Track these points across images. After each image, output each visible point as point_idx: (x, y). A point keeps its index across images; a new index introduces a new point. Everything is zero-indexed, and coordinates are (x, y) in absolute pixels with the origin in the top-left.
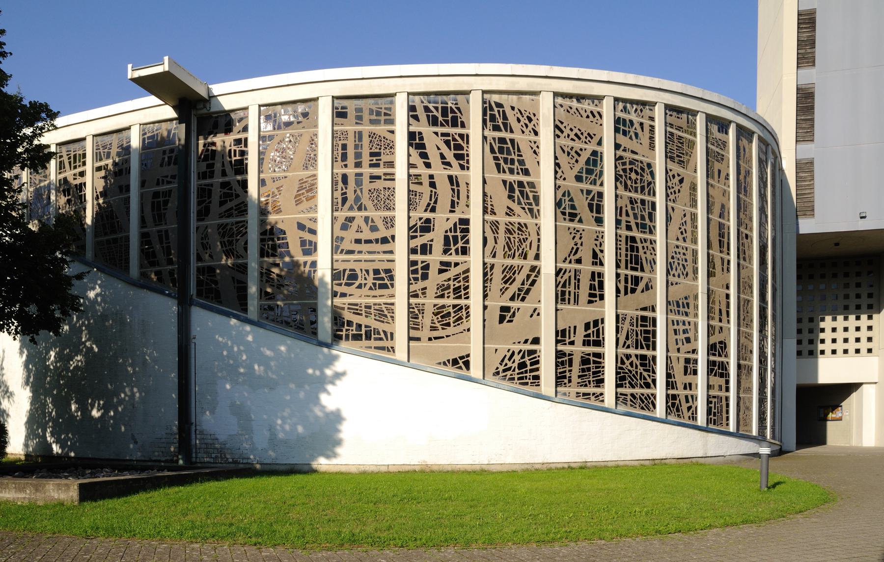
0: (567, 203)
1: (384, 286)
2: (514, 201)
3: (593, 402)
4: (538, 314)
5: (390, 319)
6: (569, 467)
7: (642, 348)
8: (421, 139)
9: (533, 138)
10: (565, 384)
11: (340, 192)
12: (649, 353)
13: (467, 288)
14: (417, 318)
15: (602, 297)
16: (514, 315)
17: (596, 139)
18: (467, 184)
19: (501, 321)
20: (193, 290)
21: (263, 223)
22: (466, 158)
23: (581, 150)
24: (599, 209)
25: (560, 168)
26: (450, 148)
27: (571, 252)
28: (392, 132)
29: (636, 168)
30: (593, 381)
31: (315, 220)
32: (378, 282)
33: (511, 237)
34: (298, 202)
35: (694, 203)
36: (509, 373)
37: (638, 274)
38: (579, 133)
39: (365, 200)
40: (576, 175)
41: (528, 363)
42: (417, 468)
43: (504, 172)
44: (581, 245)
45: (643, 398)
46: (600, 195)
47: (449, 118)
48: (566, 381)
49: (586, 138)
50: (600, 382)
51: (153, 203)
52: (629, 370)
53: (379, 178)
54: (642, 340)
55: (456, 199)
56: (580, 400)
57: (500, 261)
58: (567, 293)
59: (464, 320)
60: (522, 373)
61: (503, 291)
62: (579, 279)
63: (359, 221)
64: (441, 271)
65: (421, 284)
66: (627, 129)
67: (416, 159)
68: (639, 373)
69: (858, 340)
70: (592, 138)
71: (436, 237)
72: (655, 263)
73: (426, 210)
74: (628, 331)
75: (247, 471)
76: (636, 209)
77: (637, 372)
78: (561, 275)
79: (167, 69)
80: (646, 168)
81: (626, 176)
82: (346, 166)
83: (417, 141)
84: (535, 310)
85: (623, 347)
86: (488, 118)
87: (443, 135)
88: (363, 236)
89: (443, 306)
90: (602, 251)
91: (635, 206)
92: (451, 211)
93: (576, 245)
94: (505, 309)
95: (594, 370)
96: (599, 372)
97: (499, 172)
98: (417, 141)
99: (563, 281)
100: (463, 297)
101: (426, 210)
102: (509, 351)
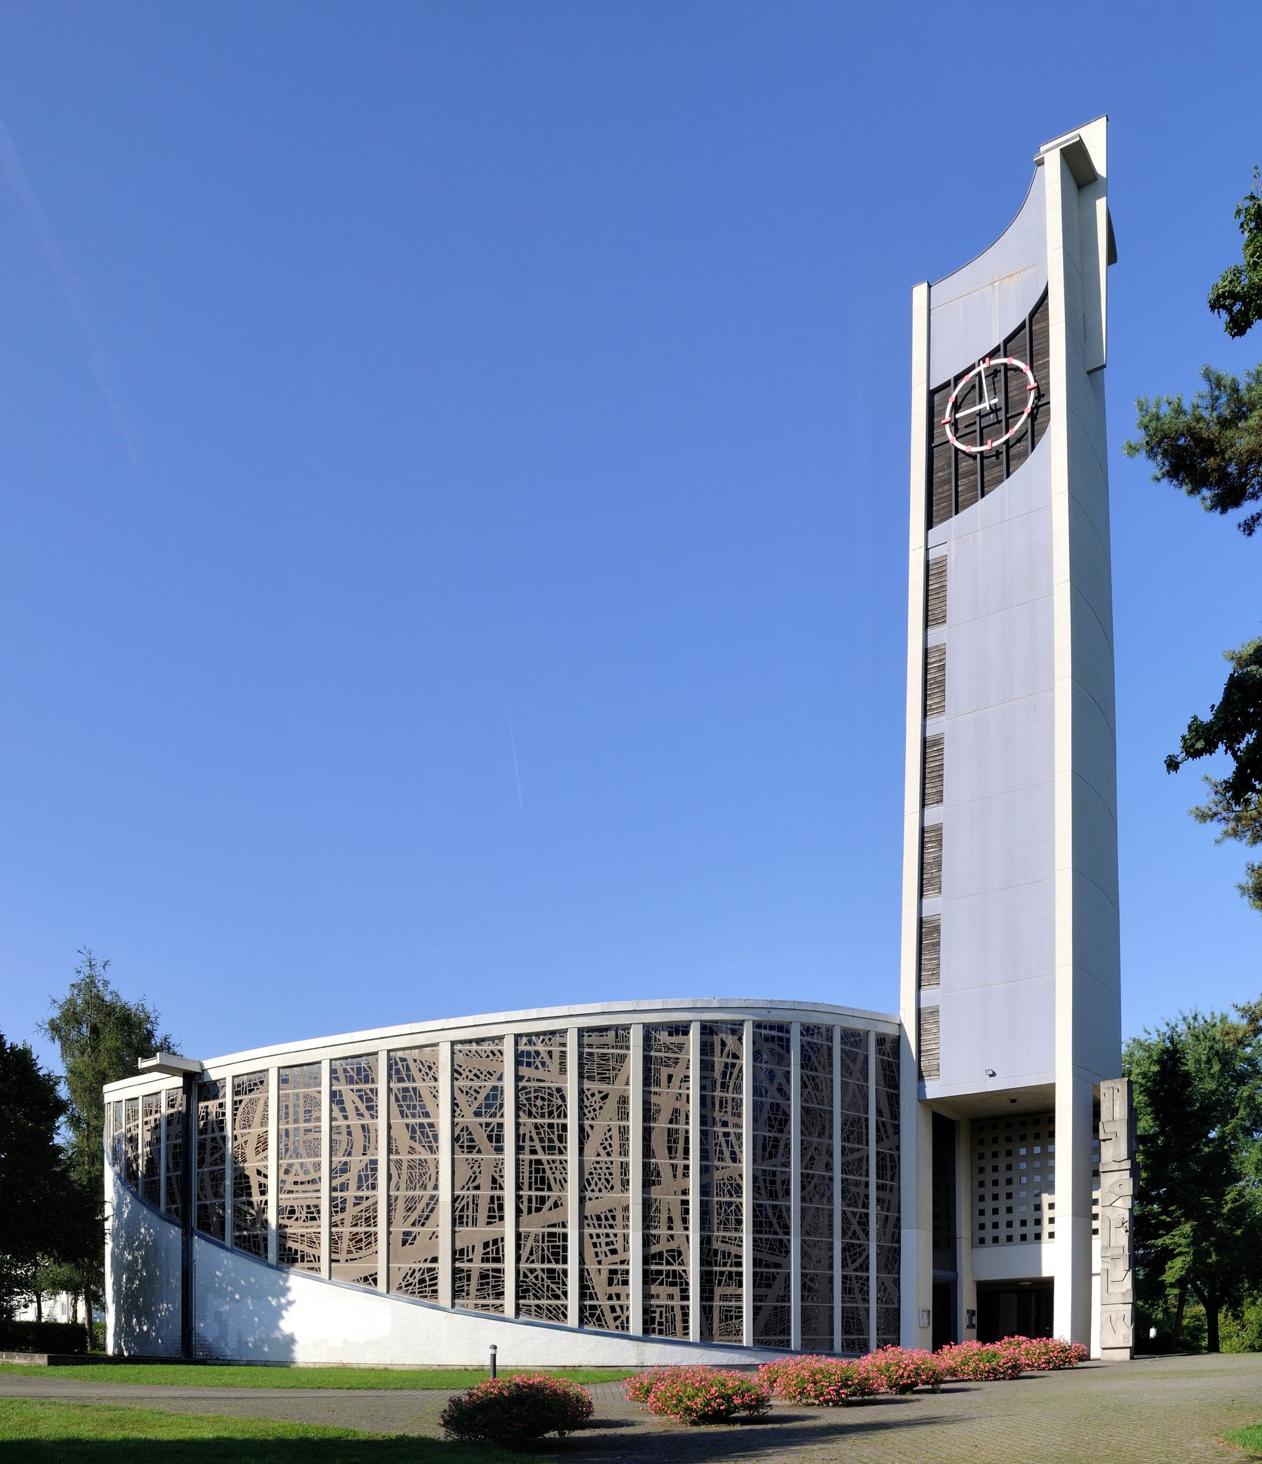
0: (465, 1137)
1: (313, 1219)
2: (415, 1141)
3: (492, 1313)
4: (437, 1237)
7: (549, 1261)
9: (433, 1084)
12: (559, 1267)
13: (375, 1217)
15: (502, 1218)
16: (415, 1238)
17: (496, 1076)
23: (480, 1087)
24: (499, 1139)
28: (320, 1092)
29: (543, 1095)
31: (266, 1167)
32: (309, 1215)
33: (413, 1172)
34: (258, 1153)
35: (624, 1115)
36: (410, 1288)
37: (545, 1193)
38: (478, 1073)
39: (302, 1151)
41: (427, 1279)
43: (407, 1117)
45: (551, 1309)
48: (464, 1294)
49: (486, 1076)
50: (500, 1295)
53: (310, 1130)
54: (550, 1255)
55: (367, 1144)
57: (403, 1193)
58: (465, 1217)
59: (373, 1244)
60: (422, 1288)
62: (477, 1205)
63: (297, 1167)
64: (355, 1205)
65: (340, 1216)
66: (532, 1060)
67: (337, 1113)
70: (491, 1075)
71: (352, 1176)
72: (566, 1181)
73: (344, 1155)
75: (228, 1363)
77: (543, 1285)
78: (459, 1201)
81: (530, 1105)
82: (288, 1122)
84: (434, 1233)
85: (526, 1262)
86: (393, 1072)
87: (357, 1091)
88: (299, 1179)
89: (357, 1234)
90: (502, 1177)
91: (542, 1130)
92: (364, 1154)
93: (474, 1173)
94: (407, 1234)
96: (499, 1285)
97: (403, 1117)
99: (460, 1206)
101: (344, 1155)
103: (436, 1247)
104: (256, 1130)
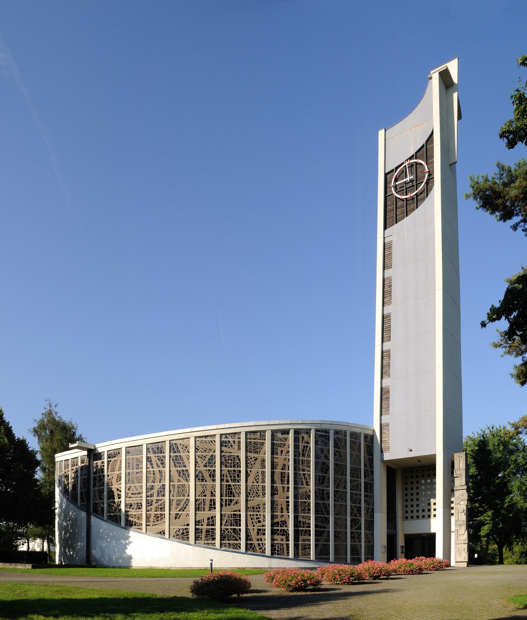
0: (200, 475)
1: (139, 508)
2: (180, 477)
3: (211, 546)
4: (189, 516)
6: (200, 569)
7: (234, 526)
8: (151, 459)
9: (187, 454)
11: (128, 478)
12: (238, 528)
13: (164, 508)
15: (215, 508)
16: (180, 516)
20: (92, 510)
23: (206, 455)
24: (214, 476)
25: (197, 463)
26: (159, 461)
31: (121, 487)
32: (138, 507)
34: (117, 482)
35: (264, 467)
36: (178, 536)
38: (205, 449)
41: (185, 533)
42: (148, 568)
43: (177, 467)
44: (206, 490)
46: (214, 471)
48: (200, 539)
50: (214, 539)
52: (227, 534)
53: (138, 473)
55: (161, 478)
56: (205, 546)
57: (175, 498)
58: (200, 507)
59: (163, 519)
60: (183, 536)
61: (176, 508)
62: (205, 502)
63: (133, 487)
64: (156, 503)
65: (150, 507)
66: (227, 444)
67: (149, 466)
69: (412, 512)
70: (211, 450)
71: (155, 491)
72: (240, 493)
73: (152, 483)
77: (231, 535)
78: (198, 501)
80: (236, 458)
82: (129, 469)
84: (188, 514)
85: (225, 526)
86: (172, 449)
88: (134, 492)
89: (157, 514)
90: (215, 491)
93: (204, 490)
94: (177, 514)
96: (214, 535)
97: (175, 467)
99: (198, 503)
101: (152, 483)
103: (189, 520)
104: (117, 472)
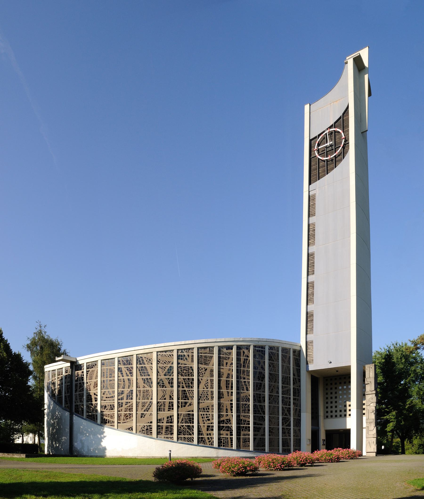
0: (161, 382)
1: (112, 409)
2: (145, 384)
3: (169, 440)
4: (152, 415)
5: (114, 418)
7: (188, 423)
8: (121, 369)
9: (151, 365)
10: (160, 434)
11: (103, 385)
12: (191, 425)
13: (132, 409)
14: (120, 417)
15: (173, 409)
16: (145, 415)
17: (171, 363)
18: (133, 380)
19: (141, 417)
20: (74, 411)
21: (87, 393)
22: (132, 373)
23: (166, 366)
24: (172, 383)
25: (159, 373)
27: (162, 397)
30: (170, 433)
31: (97, 392)
32: (111, 408)
34: (94, 388)
35: (212, 376)
36: (143, 432)
38: (165, 362)
40: (164, 374)
41: (149, 429)
43: (143, 376)
45: (189, 438)
46: (172, 379)
47: (128, 363)
48: (161, 433)
49: (168, 363)
50: (172, 434)
51: (67, 388)
53: (111, 380)
55: (130, 385)
56: (165, 439)
57: (141, 401)
59: (131, 417)
60: (147, 431)
61: (142, 409)
62: (165, 404)
63: (107, 392)
64: (126, 404)
65: (121, 408)
66: (183, 358)
67: (120, 375)
68: (187, 431)
70: (170, 362)
71: (125, 395)
72: (193, 397)
73: (122, 388)
74: (182, 418)
76: (186, 381)
77: (186, 431)
78: (159, 403)
79: (62, 358)
80: (190, 368)
82: (104, 378)
83: (120, 370)
84: (151, 414)
85: (181, 423)
86: (138, 361)
88: (107, 396)
89: (126, 414)
90: (173, 395)
92: (129, 388)
93: (164, 394)
94: (142, 414)
95: (170, 430)
96: (172, 431)
97: (141, 376)
98: (120, 370)
99: (159, 405)
100: (131, 411)
101: (122, 388)
102: (143, 425)
103: (152, 418)
104: (94, 380)
